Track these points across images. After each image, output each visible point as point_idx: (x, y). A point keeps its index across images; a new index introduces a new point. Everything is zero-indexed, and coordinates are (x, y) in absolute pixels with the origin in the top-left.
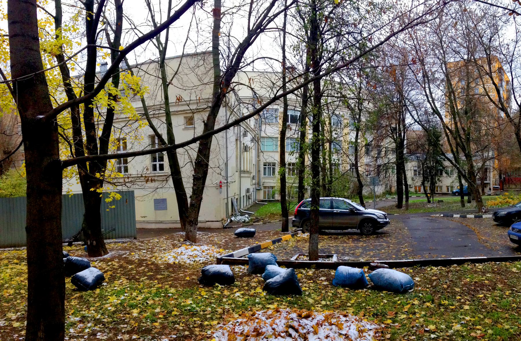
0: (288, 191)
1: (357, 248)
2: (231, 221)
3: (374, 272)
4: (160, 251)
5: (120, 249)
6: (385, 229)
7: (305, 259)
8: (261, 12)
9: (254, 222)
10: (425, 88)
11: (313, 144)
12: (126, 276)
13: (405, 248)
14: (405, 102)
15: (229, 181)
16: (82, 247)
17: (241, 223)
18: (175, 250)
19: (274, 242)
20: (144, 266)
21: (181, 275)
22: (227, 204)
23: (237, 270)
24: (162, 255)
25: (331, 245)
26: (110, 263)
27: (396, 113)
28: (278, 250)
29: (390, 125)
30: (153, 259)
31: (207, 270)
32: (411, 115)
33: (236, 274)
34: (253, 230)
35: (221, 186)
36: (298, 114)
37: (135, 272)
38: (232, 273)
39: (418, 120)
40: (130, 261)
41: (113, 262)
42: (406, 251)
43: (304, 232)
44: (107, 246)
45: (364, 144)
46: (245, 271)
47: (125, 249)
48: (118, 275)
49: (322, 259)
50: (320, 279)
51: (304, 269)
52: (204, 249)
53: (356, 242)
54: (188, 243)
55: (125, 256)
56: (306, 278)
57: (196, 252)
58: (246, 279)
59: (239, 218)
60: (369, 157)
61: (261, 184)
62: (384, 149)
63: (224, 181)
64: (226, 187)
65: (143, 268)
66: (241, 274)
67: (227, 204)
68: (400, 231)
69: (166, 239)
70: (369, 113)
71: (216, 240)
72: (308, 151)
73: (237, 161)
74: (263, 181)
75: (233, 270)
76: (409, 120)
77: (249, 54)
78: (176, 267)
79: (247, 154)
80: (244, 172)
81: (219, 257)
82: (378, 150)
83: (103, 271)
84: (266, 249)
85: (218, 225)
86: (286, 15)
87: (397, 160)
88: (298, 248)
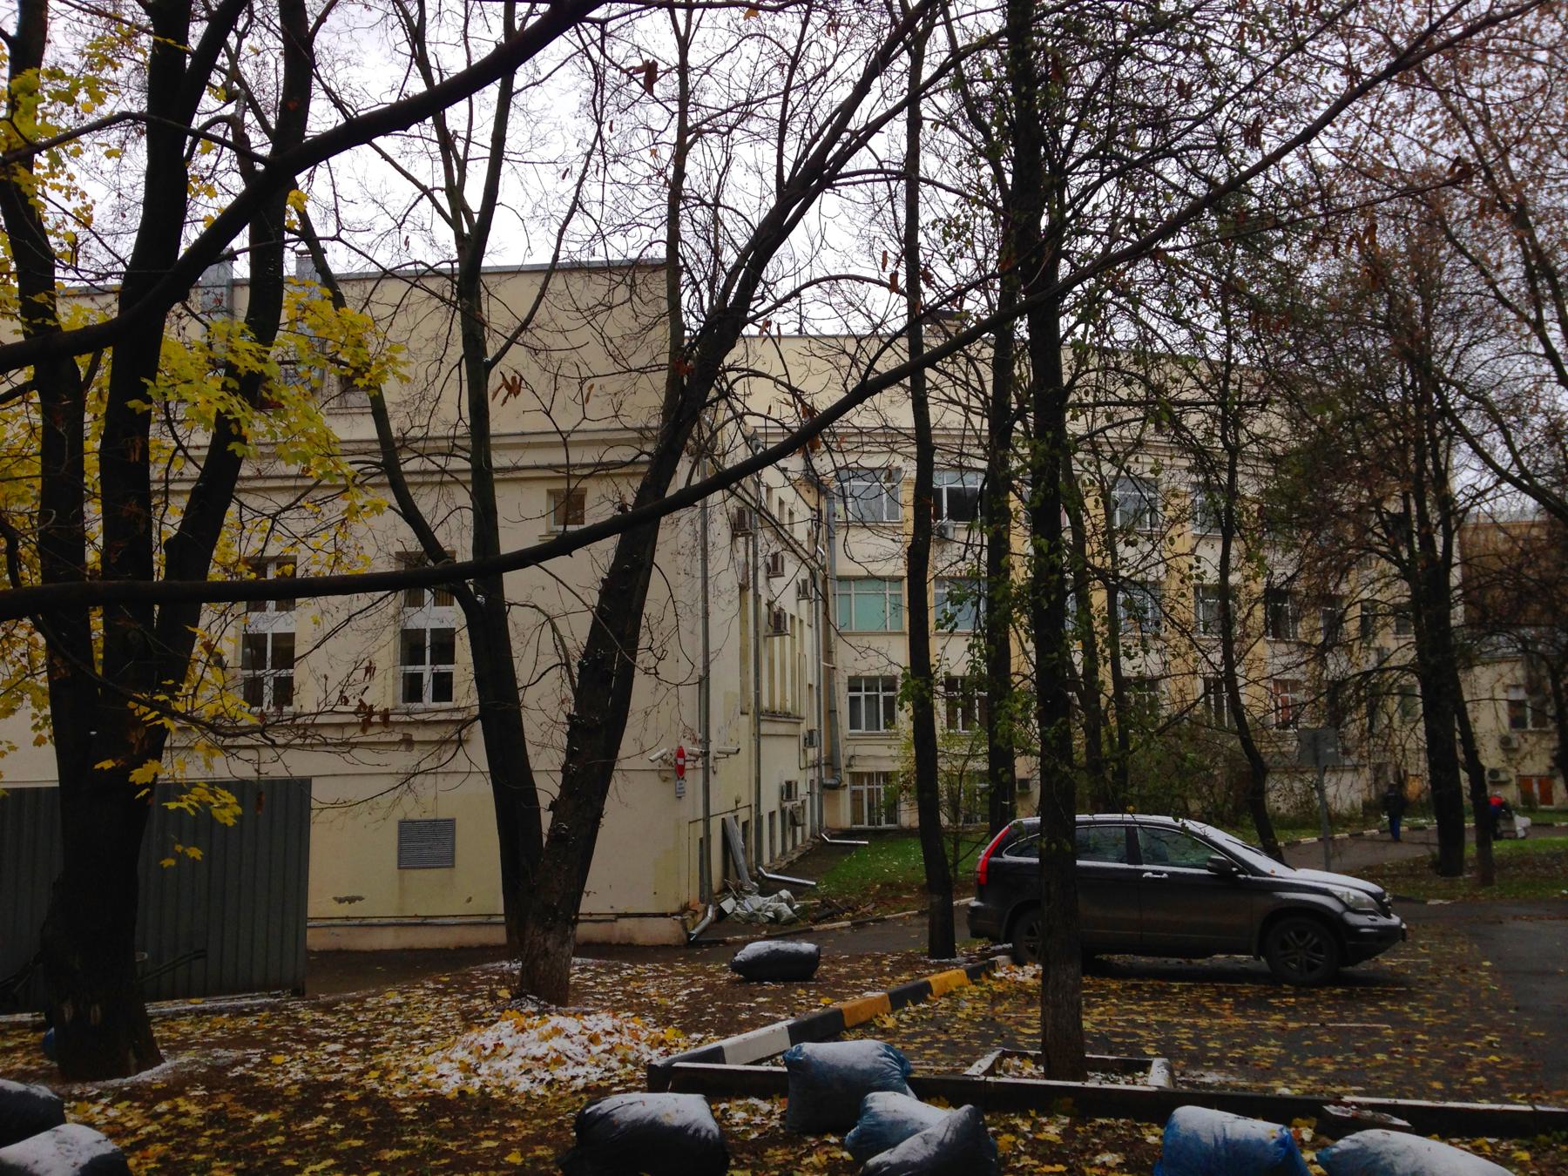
0: (951, 792)
1: (1258, 1035)
2: (721, 914)
3: (1343, 1144)
4: (407, 1042)
5: (221, 1043)
6: (1387, 962)
7: (1029, 1074)
8: (821, 120)
9: (816, 921)
10: (1538, 326)
11: (1035, 585)
12: (237, 1158)
13: (1486, 1054)
14: (1443, 399)
15: (713, 748)
16: (30, 1038)
17: (762, 926)
18: (472, 1036)
19: (897, 1000)
20: (324, 1112)
21: (486, 1144)
22: (705, 843)
23: (740, 1116)
24: (411, 1061)
25: (1141, 1019)
26: (163, 1107)
27: (1403, 450)
28: (915, 1035)
29: (1378, 503)
30: (371, 1080)
31: (607, 1116)
32: (1478, 451)
33: (734, 1135)
34: (807, 947)
35: (680, 771)
36: (975, 482)
37: (279, 1139)
38: (716, 1131)
39: (1515, 472)
40: (265, 1091)
41: (180, 1101)
42: (1494, 1065)
43: (1019, 962)
44: (158, 1032)
45: (1258, 587)
46: (775, 1123)
47: (244, 1040)
48: (199, 1157)
49: (1100, 1076)
50: (1098, 1159)
51: (1025, 1117)
52: (598, 1030)
53: (1251, 1012)
54: (530, 1008)
55: (239, 1070)
56: (1033, 1155)
57: (559, 1043)
58: (778, 1155)
59: (755, 902)
60: (1282, 647)
61: (843, 763)
62: (1356, 611)
63: (691, 748)
64: (700, 775)
65: (321, 1119)
66: (754, 1135)
67: (705, 843)
68: (1460, 978)
69: (438, 991)
70: (1273, 459)
71: (652, 991)
72: (1015, 613)
73: (743, 672)
74: (850, 752)
75: (722, 1118)
76: (1466, 475)
77: (783, 269)
78: (467, 1111)
79: (782, 644)
80: (773, 715)
81: (660, 1062)
82: (1327, 615)
83: (127, 1142)
84: (866, 1027)
85: (664, 931)
86: (915, 124)
87: (1420, 654)
88: (998, 1027)
